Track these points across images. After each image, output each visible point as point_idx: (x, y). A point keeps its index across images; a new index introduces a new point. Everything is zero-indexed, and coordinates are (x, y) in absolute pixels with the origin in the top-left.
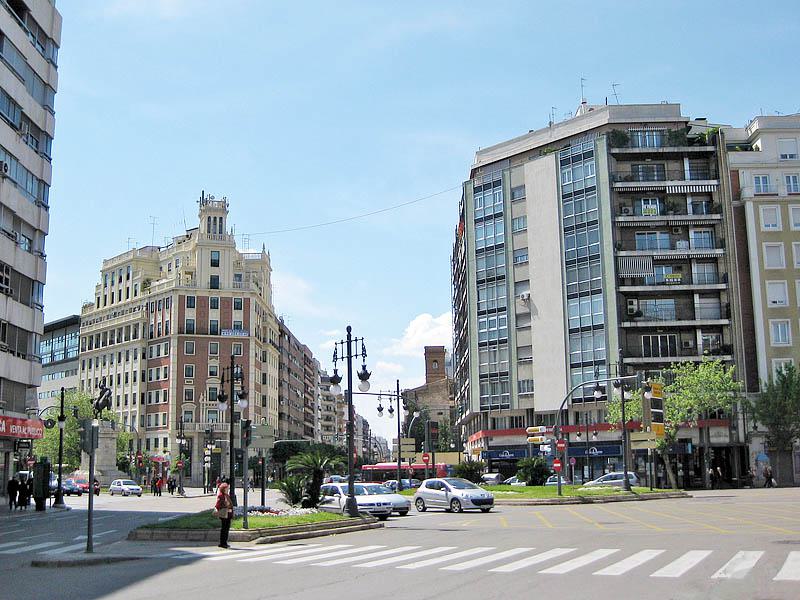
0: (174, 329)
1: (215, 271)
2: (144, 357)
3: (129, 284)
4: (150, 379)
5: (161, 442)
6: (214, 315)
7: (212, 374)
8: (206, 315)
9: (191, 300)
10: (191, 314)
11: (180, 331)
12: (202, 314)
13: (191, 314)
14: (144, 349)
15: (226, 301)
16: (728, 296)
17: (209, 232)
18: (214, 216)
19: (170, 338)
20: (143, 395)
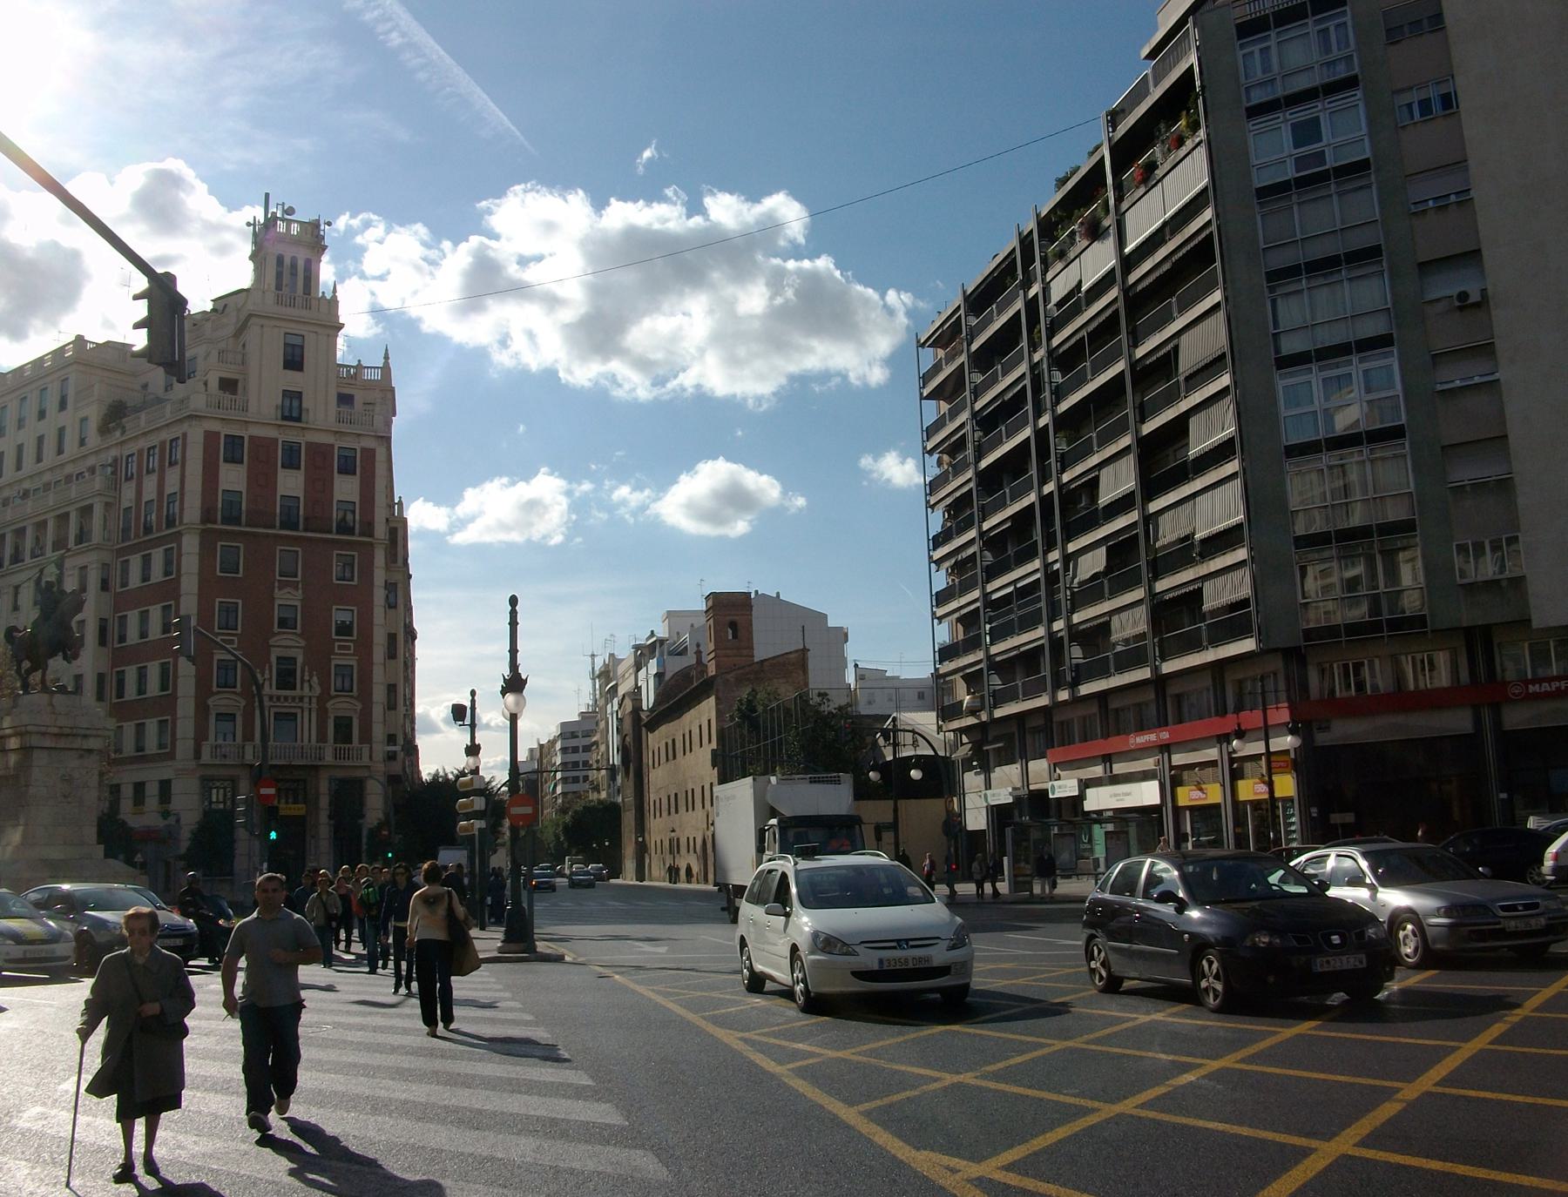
0: (192, 511)
1: (293, 380)
2: (103, 640)
3: (68, 419)
4: (122, 638)
5: (152, 790)
6: (291, 483)
7: (283, 623)
8: (272, 484)
9: (234, 442)
10: (233, 478)
11: (208, 515)
12: (262, 480)
13: (233, 478)
14: (105, 566)
15: (320, 453)
16: (921, 394)
17: (279, 287)
18: (359, 361)
19: (179, 534)
20: (101, 678)
